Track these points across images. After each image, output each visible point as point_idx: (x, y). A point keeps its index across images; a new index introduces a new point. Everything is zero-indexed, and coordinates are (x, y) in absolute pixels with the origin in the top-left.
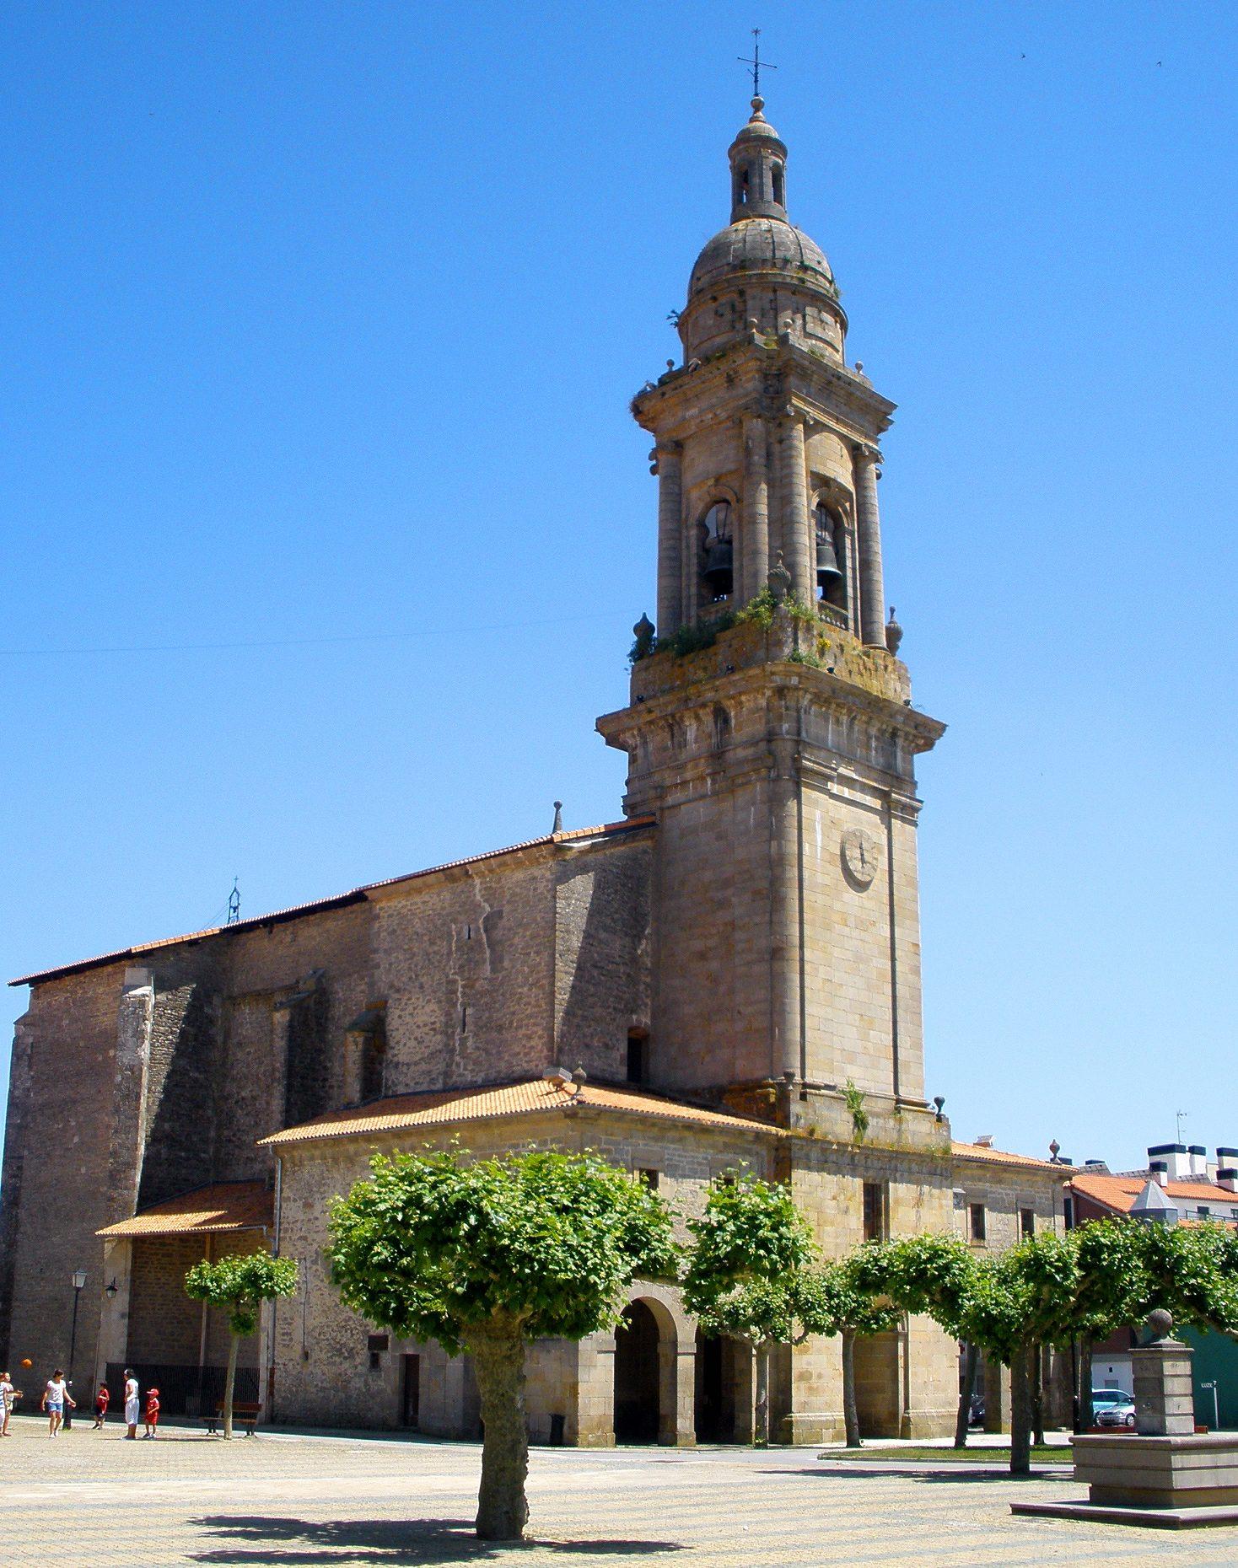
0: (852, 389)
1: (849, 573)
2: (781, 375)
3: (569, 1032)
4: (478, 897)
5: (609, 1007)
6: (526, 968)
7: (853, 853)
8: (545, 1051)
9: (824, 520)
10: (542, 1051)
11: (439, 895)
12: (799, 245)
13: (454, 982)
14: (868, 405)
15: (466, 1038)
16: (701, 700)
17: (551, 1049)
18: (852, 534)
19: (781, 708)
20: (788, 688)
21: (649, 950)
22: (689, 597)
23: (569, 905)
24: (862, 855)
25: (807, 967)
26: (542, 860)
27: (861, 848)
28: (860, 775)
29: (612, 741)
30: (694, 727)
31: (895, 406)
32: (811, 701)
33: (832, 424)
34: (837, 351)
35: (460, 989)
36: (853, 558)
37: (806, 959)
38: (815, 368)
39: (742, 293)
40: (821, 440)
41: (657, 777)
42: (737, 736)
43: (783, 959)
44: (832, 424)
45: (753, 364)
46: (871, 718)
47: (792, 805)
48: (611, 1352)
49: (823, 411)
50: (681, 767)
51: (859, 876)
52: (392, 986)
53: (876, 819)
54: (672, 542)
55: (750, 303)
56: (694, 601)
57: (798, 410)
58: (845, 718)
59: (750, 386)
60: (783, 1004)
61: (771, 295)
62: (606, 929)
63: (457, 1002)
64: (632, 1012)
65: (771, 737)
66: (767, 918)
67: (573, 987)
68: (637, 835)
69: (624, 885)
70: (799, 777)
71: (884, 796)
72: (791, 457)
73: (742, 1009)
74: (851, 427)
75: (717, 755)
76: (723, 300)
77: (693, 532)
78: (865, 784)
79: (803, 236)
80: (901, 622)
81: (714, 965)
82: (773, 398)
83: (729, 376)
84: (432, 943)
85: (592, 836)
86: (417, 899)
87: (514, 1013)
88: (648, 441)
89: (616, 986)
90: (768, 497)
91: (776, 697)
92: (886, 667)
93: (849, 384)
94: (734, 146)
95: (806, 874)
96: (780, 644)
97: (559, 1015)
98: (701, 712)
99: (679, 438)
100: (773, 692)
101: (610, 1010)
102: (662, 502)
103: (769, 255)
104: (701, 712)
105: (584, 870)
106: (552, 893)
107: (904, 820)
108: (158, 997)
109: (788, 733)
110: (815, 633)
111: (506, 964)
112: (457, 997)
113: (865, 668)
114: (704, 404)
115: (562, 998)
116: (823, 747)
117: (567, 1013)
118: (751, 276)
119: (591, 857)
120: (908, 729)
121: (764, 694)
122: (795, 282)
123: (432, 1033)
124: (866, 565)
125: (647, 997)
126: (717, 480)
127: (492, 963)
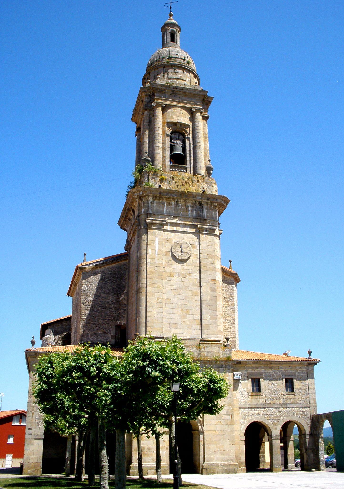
0: (184, 91)
5: (106, 319)
14: (194, 94)
19: (142, 204)
20: (142, 197)
21: (125, 298)
23: (88, 287)
24: (182, 250)
25: (148, 294)
27: (181, 247)
31: (207, 92)
32: (153, 199)
36: (190, 147)
38: (164, 88)
40: (171, 111)
46: (185, 200)
47: (144, 237)
48: (243, 440)
49: (172, 101)
51: (180, 258)
53: (193, 236)
62: (104, 293)
67: (89, 314)
70: (147, 227)
71: (195, 227)
72: (155, 119)
74: (187, 103)
78: (186, 224)
85: (97, 262)
89: (109, 312)
90: (149, 135)
92: (198, 181)
93: (182, 89)
95: (149, 260)
101: (107, 320)
105: (95, 274)
108: (55, 337)
109: (144, 212)
110: (159, 175)
113: (186, 183)
117: (86, 323)
119: (98, 270)
120: (206, 201)
121: (136, 201)
125: (125, 314)
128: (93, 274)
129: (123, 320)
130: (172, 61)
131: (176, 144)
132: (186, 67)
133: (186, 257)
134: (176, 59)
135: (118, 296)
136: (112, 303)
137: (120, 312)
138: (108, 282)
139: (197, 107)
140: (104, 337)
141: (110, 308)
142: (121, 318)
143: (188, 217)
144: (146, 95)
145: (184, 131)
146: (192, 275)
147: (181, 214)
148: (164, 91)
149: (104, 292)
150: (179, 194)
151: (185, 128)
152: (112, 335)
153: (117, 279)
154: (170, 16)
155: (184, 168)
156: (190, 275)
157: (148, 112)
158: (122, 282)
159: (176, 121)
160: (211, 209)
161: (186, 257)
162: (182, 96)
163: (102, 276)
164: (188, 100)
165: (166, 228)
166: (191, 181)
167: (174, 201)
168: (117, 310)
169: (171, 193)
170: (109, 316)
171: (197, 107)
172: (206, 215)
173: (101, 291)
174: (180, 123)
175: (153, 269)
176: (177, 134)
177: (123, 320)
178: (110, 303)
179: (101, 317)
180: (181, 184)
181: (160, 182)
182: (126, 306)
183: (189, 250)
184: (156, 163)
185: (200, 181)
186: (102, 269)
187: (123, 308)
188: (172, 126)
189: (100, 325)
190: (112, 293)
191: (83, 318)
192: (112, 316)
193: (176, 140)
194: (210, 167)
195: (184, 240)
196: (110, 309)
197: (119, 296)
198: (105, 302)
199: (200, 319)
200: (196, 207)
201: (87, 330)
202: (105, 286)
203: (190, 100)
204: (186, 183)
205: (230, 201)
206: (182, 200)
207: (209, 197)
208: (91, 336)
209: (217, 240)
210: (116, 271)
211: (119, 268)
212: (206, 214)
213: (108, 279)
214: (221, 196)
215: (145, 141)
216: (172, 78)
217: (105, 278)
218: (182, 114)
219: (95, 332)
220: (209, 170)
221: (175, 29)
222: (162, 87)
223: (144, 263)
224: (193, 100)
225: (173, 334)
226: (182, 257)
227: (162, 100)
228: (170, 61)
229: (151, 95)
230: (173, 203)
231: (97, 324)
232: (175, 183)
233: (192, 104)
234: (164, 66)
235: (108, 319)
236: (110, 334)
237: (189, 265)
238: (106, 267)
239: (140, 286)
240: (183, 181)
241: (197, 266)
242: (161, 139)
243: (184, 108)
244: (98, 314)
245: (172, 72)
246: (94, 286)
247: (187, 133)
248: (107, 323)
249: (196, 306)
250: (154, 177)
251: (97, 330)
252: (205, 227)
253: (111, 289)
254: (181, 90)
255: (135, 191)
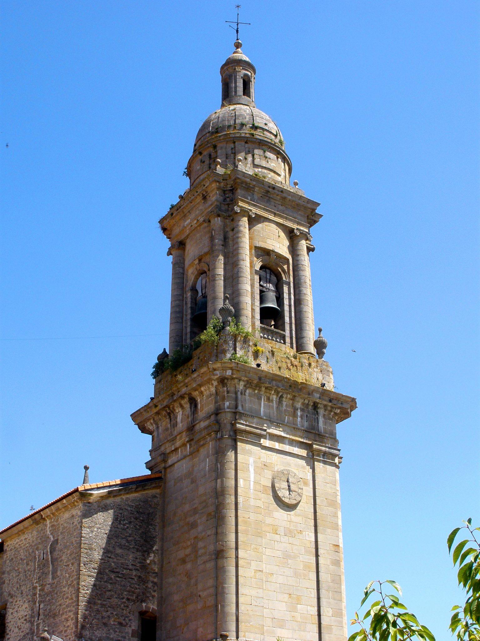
0: (284, 195)
1: (286, 308)
2: (233, 190)
3: (90, 615)
4: (48, 532)
5: (123, 598)
6: (67, 574)
7: (281, 487)
8: (74, 628)
9: (268, 277)
10: (72, 629)
11: (32, 534)
12: (253, 115)
13: (35, 588)
14: (298, 205)
15: (39, 624)
16: (180, 393)
17: (76, 627)
18: (289, 284)
19: (224, 392)
20: (227, 379)
21: (156, 560)
22: (186, 334)
23: (92, 532)
24: (289, 486)
25: (241, 562)
26: (76, 503)
27: (288, 481)
28: (288, 433)
29: (144, 430)
30: (181, 413)
31: (319, 204)
32: (245, 386)
33: (271, 217)
34: (279, 175)
35: (38, 592)
36: (290, 299)
37: (239, 556)
38: (254, 183)
39: (215, 147)
40: (262, 228)
41: (162, 449)
42: (201, 414)
43: (223, 557)
44: (271, 217)
45: (214, 185)
46: (295, 396)
47: (231, 455)
49: (264, 209)
50: (174, 440)
51: (287, 500)
52: (10, 594)
53: (303, 462)
54: (177, 302)
55: (219, 152)
56: (188, 336)
57: (242, 208)
58: (275, 397)
59: (214, 199)
60: (223, 588)
61: (232, 145)
62: (121, 546)
63: (36, 601)
64: (142, 601)
65: (217, 412)
66: (214, 531)
67: (94, 585)
68: (145, 485)
69: (136, 519)
71: (308, 447)
72: (238, 237)
73: (201, 593)
74: (286, 218)
75: (191, 429)
76: (205, 153)
77: (189, 294)
78: (293, 440)
79: (256, 111)
80: (325, 338)
81: (189, 566)
82: (228, 204)
83: (203, 195)
84: (28, 564)
85: (110, 486)
86: (23, 538)
87: (60, 605)
88: (168, 244)
89: (128, 584)
90: (225, 264)
91: (221, 386)
92: (310, 365)
93: (282, 192)
94: (222, 68)
95: (240, 499)
96: (224, 352)
97: (82, 604)
98: (183, 402)
99: (181, 239)
100: (218, 382)
101: (124, 600)
102: (173, 279)
103: (232, 122)
104: (183, 402)
105: (105, 509)
106: (80, 524)
107: (325, 463)
109: (228, 408)
110: (251, 343)
111: (59, 573)
112: (37, 597)
113: (292, 365)
114: (193, 216)
115: (85, 592)
116: (255, 415)
117: (89, 602)
118: (220, 136)
119: (110, 501)
120: (325, 403)
121: (212, 384)
122: (248, 135)
123: (25, 622)
124: (298, 302)
125: (155, 591)
126: (200, 260)
127: (52, 574)
128: (102, 508)
129: (152, 602)
130: (258, 134)
131: (267, 289)
132: (281, 151)
133: (295, 500)
134: (265, 132)
135: (143, 556)
136: (134, 567)
137: (146, 587)
138: (128, 527)
139: (302, 228)
140: (120, 632)
141: (131, 577)
142: (148, 597)
143: (296, 427)
144: (218, 188)
145: (280, 268)
146: (304, 533)
147: (286, 421)
148: (254, 188)
149: (121, 545)
150: (288, 385)
151: (282, 263)
152: (133, 630)
153: (141, 523)
154: (237, 47)
155: (280, 336)
156: (300, 533)
157: (221, 221)
158: (150, 529)
159: (271, 248)
160: (330, 419)
161: (295, 500)
162: (279, 203)
163: (116, 514)
164: (287, 212)
165: (263, 441)
166: (300, 362)
167: (277, 396)
168: (142, 581)
169: (276, 380)
170: (129, 591)
171: (302, 228)
172: (323, 427)
173: (116, 542)
174: (276, 252)
175: (247, 516)
176: (267, 270)
177: (152, 602)
178: (131, 567)
179: (116, 593)
180: (284, 365)
181: (254, 357)
182: (157, 575)
183: (300, 488)
184: (243, 319)
185: (313, 364)
186: (117, 501)
187: (151, 579)
188: (262, 256)
189: (113, 608)
190: (133, 548)
191: (84, 592)
192: (134, 592)
193: (267, 282)
194: (324, 343)
195: (290, 469)
196: (130, 580)
197: (146, 556)
198: (122, 564)
199: (316, 613)
200: (308, 412)
201: (90, 615)
202: (121, 534)
203: (291, 214)
204: (292, 365)
205: (357, 407)
206: (289, 396)
207: (331, 397)
208: (98, 629)
209: (337, 472)
210: (140, 506)
211: (146, 501)
212: (323, 425)
213: (127, 522)
214: (350, 398)
215: (218, 275)
216: (260, 166)
217: (123, 519)
218: (279, 236)
219: (104, 621)
220: (320, 346)
221: (250, 74)
222: (251, 180)
223: (231, 503)
224: (295, 215)
225: (278, 638)
226: (289, 499)
227: (248, 203)
228: (256, 134)
229: (227, 190)
230: (274, 399)
231: (109, 607)
232: (277, 362)
233: (294, 222)
234: (247, 141)
235: (126, 597)
236: (130, 626)
237: (299, 515)
238: (124, 497)
239: (223, 546)
240: (288, 361)
241: (311, 518)
242: (249, 277)
243: (281, 226)
244: (109, 586)
245: (260, 155)
246: (103, 531)
247: (284, 273)
248: (125, 606)
249: (310, 590)
250: (244, 346)
251: (109, 617)
252: (323, 448)
253: (132, 541)
254: (280, 193)
255: (219, 367)
